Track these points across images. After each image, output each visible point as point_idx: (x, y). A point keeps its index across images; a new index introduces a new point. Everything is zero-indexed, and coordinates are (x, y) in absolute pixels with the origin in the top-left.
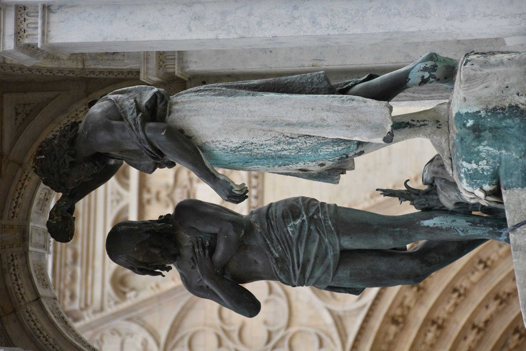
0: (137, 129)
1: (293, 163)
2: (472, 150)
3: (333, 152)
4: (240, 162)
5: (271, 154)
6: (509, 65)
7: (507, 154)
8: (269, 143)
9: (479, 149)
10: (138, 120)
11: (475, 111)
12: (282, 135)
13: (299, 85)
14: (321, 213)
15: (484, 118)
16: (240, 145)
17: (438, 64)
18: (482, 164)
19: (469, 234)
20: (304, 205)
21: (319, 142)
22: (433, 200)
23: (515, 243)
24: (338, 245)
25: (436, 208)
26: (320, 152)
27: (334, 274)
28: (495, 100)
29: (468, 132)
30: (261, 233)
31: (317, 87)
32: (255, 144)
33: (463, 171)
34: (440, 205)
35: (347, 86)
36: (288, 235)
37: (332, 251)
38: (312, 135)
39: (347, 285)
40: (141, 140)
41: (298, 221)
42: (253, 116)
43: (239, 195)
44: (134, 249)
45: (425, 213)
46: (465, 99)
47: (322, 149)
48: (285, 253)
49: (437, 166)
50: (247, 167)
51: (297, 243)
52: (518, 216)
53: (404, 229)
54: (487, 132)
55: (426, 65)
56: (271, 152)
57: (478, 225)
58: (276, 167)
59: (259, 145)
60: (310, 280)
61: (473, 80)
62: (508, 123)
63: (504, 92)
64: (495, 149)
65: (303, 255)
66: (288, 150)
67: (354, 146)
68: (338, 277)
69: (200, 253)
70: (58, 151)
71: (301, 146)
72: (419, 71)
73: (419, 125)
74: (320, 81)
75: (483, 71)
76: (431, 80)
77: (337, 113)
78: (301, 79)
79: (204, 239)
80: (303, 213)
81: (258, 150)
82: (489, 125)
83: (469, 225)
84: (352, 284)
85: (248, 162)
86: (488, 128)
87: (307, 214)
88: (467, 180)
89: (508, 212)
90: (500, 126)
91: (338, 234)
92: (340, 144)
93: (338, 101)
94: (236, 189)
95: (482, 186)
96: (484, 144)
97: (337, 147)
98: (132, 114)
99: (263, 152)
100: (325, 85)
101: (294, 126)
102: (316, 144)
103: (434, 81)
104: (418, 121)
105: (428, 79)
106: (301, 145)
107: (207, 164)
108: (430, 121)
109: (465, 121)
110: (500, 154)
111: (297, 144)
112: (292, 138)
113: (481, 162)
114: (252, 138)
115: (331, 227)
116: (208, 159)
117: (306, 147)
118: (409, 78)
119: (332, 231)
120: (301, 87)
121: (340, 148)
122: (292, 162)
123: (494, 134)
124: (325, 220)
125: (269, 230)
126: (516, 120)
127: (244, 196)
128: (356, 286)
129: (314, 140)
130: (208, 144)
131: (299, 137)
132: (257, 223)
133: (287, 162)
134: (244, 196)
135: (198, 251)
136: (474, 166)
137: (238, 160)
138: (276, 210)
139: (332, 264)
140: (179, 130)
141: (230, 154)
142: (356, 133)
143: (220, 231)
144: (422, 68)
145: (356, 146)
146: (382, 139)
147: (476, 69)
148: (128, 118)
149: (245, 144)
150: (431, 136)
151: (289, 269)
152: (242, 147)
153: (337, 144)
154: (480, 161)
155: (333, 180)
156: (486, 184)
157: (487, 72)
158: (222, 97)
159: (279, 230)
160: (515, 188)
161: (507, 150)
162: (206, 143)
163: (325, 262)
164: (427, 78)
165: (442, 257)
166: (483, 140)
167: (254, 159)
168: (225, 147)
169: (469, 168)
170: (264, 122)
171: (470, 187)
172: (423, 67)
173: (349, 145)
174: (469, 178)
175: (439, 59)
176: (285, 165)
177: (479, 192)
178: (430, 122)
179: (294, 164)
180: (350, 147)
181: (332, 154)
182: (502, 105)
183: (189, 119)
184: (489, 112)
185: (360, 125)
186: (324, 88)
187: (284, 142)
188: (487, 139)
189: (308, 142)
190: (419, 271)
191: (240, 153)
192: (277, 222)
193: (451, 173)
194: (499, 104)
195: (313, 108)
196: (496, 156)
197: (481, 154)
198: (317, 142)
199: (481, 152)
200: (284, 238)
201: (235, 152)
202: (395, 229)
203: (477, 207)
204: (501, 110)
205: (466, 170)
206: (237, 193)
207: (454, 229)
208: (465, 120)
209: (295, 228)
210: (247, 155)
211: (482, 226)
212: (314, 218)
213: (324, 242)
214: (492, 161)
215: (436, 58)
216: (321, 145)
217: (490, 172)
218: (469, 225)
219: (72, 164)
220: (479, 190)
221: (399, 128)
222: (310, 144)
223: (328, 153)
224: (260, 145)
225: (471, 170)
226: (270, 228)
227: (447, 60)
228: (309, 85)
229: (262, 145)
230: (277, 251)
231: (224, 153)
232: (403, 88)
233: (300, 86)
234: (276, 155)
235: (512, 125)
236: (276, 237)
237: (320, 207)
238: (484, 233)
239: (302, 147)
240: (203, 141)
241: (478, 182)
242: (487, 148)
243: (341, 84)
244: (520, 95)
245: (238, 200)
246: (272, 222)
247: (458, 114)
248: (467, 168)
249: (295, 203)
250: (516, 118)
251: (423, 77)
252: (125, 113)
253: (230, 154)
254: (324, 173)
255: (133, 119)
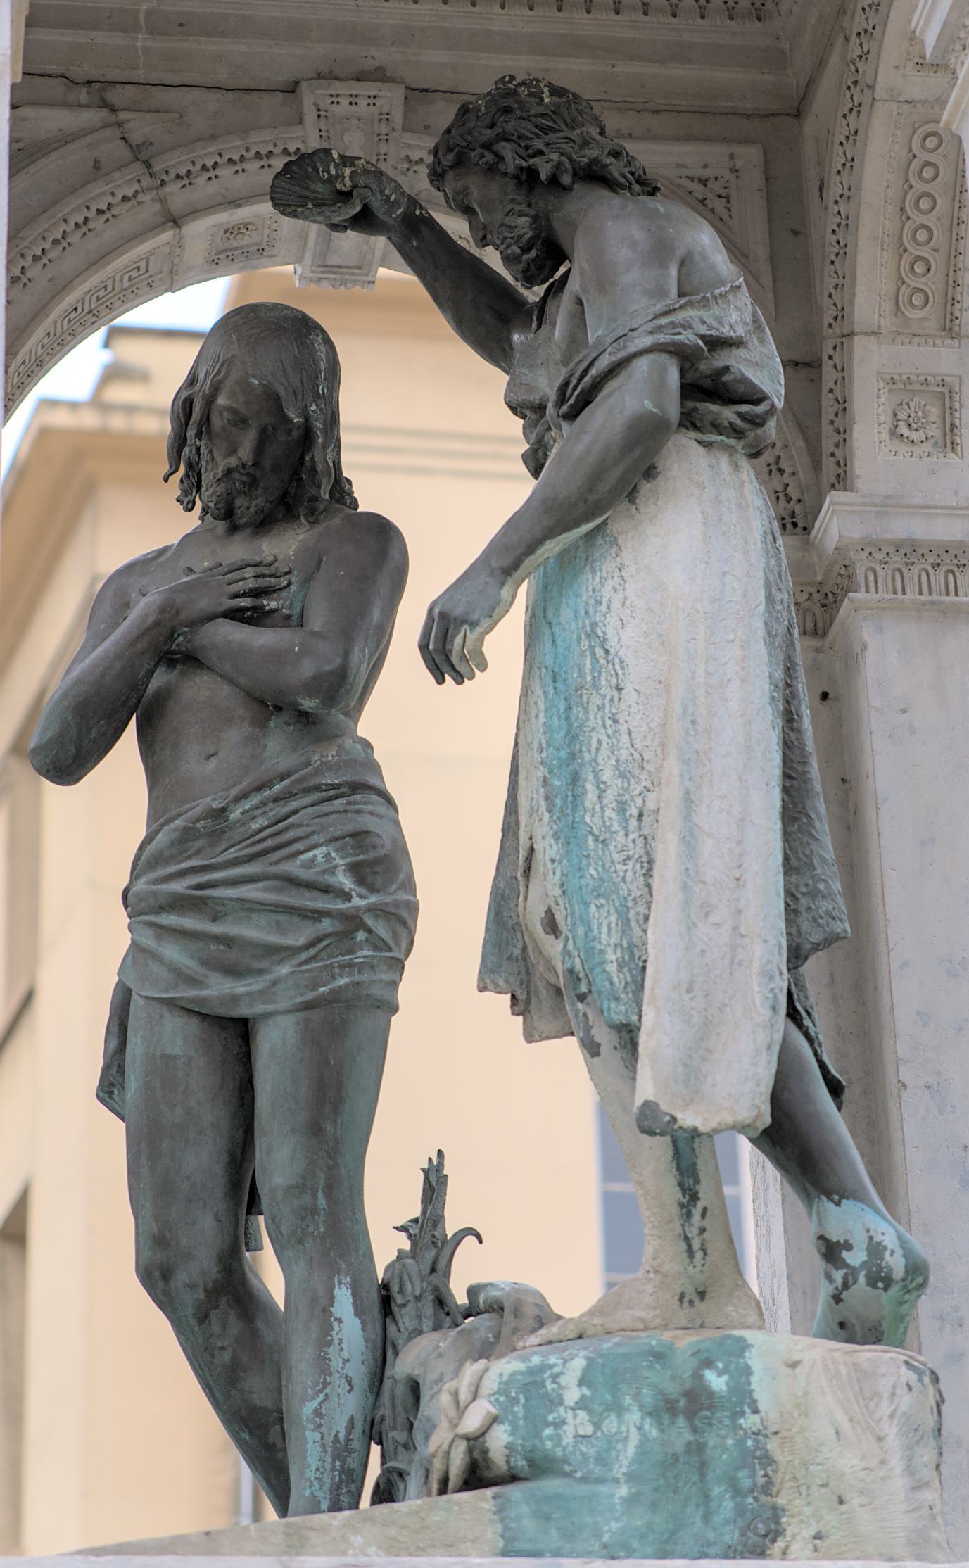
0: (660, 329)
1: (555, 822)
2: (623, 1387)
3: (598, 947)
4: (556, 657)
5: (584, 749)
6: (912, 1507)
7: (617, 1501)
8: (621, 745)
9: (628, 1410)
10: (687, 337)
11: (755, 1396)
12: (648, 784)
13: (806, 856)
14: (373, 957)
15: (736, 1427)
16: (612, 651)
17: (895, 1290)
18: (577, 1421)
19: (307, 1433)
20: (397, 904)
21: (630, 904)
22: (419, 1317)
23: (312, 1529)
24: (270, 1007)
25: (392, 1329)
26: (597, 906)
27: (171, 1004)
28: (797, 1462)
29: (685, 1376)
30: (308, 764)
31: (802, 909)
32: (616, 700)
33: (553, 1360)
34: (401, 1342)
35: (803, 1014)
36: (302, 848)
37: (248, 988)
38: (656, 883)
39: (136, 1046)
40: (625, 342)
41: (345, 881)
42: (709, 690)
43: (448, 647)
44: (254, 376)
45: (374, 1297)
46: (794, 1365)
47: (608, 912)
48: (241, 842)
49: (540, 1314)
50: (537, 681)
51: (276, 877)
52: (403, 1539)
53: (324, 1221)
54: (689, 1436)
55: (892, 1253)
56: (593, 751)
57: (338, 1463)
58: (542, 771)
59: (614, 711)
60: (149, 932)
61: (861, 1390)
62: (720, 1506)
63: (823, 1490)
64: (633, 1462)
65: (235, 896)
66: (601, 802)
67: (621, 1012)
68: (161, 1017)
69: (241, 583)
70: (567, 138)
71: (616, 847)
72: (868, 1231)
73: (689, 1235)
74: (822, 918)
75: (891, 1424)
76: (838, 1275)
77: (729, 956)
78: (823, 860)
79: (284, 594)
80: (373, 899)
81: (599, 708)
82: (711, 1443)
83: (338, 1432)
84: (138, 1062)
85: (554, 681)
86: (701, 1440)
87: (371, 909)
88: (523, 1374)
89: (419, 1506)
90: (708, 1478)
91: (308, 1006)
92: (625, 970)
93: (769, 962)
94: (471, 637)
95: (502, 1422)
96: (647, 1426)
97: (617, 960)
98: (704, 322)
99: (591, 723)
100: (810, 935)
101: (685, 818)
102: (621, 892)
103: (834, 1285)
104: (702, 1230)
105: (842, 1264)
106: (619, 846)
107: (552, 548)
108: (705, 1269)
109: (720, 1365)
110: (616, 1481)
111: (622, 833)
112: (641, 815)
113: (587, 1417)
114: (636, 687)
115: (329, 983)
116: (563, 554)
117: (612, 862)
118: (844, 1201)
119: (315, 987)
120: (799, 859)
121: (612, 968)
122: (559, 819)
123: (682, 1459)
124: (350, 965)
125: (317, 788)
126: (733, 1532)
127: (445, 667)
128: (132, 1078)
129: (637, 888)
130: (613, 552)
131: (646, 838)
132: (338, 754)
133: (558, 802)
134: (445, 667)
135: (247, 575)
136: (572, 1395)
137: (560, 650)
138: (379, 816)
139: (205, 993)
140: (653, 467)
141: (584, 623)
142: (670, 1013)
143: (313, 633)
144: (877, 1239)
145: (618, 1018)
146: (651, 1098)
147: (897, 1400)
148: (689, 309)
149: (617, 667)
150: (652, 1275)
151: (189, 857)
152: (606, 658)
153: (627, 958)
154: (590, 1412)
155: (492, 972)
156: (512, 1433)
157: (886, 1435)
158: (764, 603)
159: (317, 820)
160: (499, 1528)
161: (631, 1501)
162: (615, 548)
163: (212, 975)
164: (843, 1260)
165: (226, 1357)
166: (659, 1423)
167: (566, 699)
168: (604, 605)
169: (562, 1380)
170: (693, 722)
171: (500, 1383)
172: (885, 1243)
173: (623, 996)
174: (528, 1379)
175: (907, 1297)
176: (547, 798)
177: (484, 1413)
178: (699, 1268)
179: (551, 828)
180: (617, 999)
181: (592, 944)
182: (782, 1482)
183: (692, 495)
184: (756, 1441)
185: (696, 1028)
186: (799, 931)
187: (627, 790)
188: (665, 1438)
189: (630, 867)
190: (181, 1277)
191: (588, 653)
192: (344, 816)
193: (528, 1343)
194: (785, 1473)
195: (741, 883)
196: (606, 1465)
197: (613, 1416)
198: (629, 895)
199: (619, 1416)
200: (290, 835)
201: (588, 636)
202: (323, 1192)
203: (400, 1458)
204: (763, 1479)
205: (556, 1370)
206: (458, 640)
207: (325, 1384)
208: (726, 1366)
209: (324, 872)
210: (582, 675)
211: (333, 1478)
212: (356, 930)
213: (281, 962)
214: (592, 1452)
215: (914, 1285)
216: (620, 909)
217: (556, 1445)
218: (338, 1432)
219: (528, 179)
220: (489, 1413)
221: (678, 1168)
222: (622, 874)
223: (596, 932)
224: (613, 714)
225: (555, 1386)
226: (324, 793)
227: (902, 1330)
228: (806, 885)
229: (615, 721)
230: (249, 816)
231: (586, 602)
232: (808, 1186)
233: (801, 855)
234: (582, 765)
235: (715, 1519)
236: (296, 812)
237: (391, 954)
238: (311, 1482)
239: (612, 848)
240: (623, 536)
241: (516, 1409)
242: (634, 1438)
243: (807, 997)
244: (817, 1542)
245: (431, 647)
246: (343, 801)
247: (743, 1346)
248: (562, 1373)
249: (401, 877)
250: (737, 1530)
251: (848, 1246)
252: (704, 306)
253: (584, 623)
254: (515, 941)
255: (687, 321)
